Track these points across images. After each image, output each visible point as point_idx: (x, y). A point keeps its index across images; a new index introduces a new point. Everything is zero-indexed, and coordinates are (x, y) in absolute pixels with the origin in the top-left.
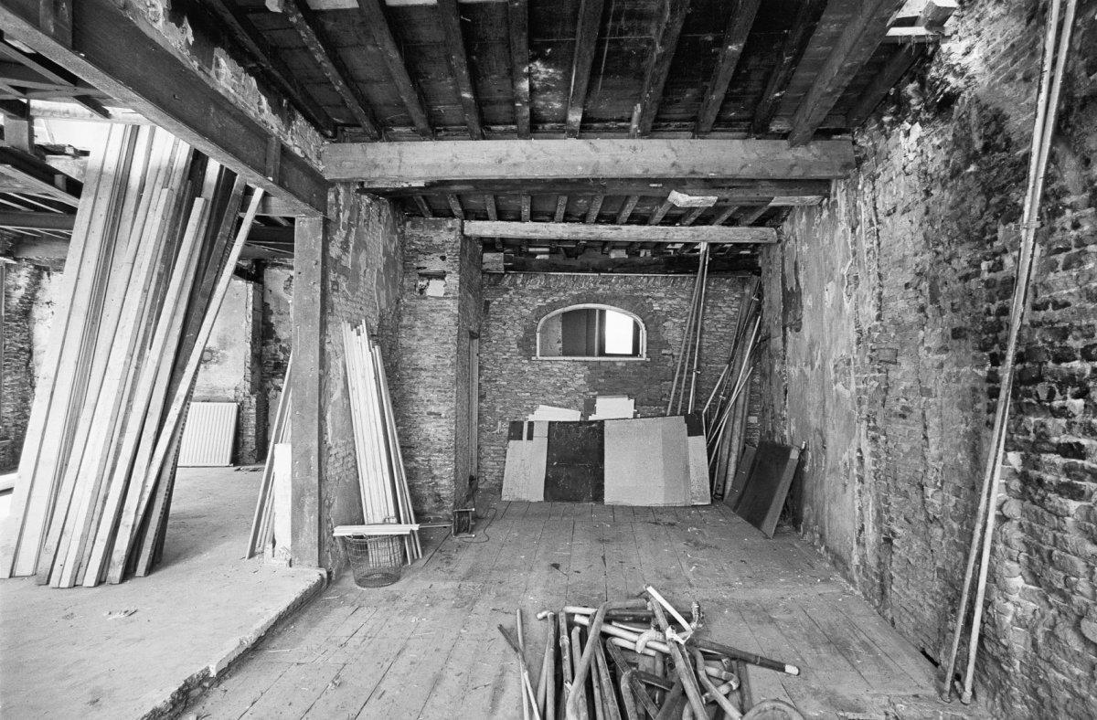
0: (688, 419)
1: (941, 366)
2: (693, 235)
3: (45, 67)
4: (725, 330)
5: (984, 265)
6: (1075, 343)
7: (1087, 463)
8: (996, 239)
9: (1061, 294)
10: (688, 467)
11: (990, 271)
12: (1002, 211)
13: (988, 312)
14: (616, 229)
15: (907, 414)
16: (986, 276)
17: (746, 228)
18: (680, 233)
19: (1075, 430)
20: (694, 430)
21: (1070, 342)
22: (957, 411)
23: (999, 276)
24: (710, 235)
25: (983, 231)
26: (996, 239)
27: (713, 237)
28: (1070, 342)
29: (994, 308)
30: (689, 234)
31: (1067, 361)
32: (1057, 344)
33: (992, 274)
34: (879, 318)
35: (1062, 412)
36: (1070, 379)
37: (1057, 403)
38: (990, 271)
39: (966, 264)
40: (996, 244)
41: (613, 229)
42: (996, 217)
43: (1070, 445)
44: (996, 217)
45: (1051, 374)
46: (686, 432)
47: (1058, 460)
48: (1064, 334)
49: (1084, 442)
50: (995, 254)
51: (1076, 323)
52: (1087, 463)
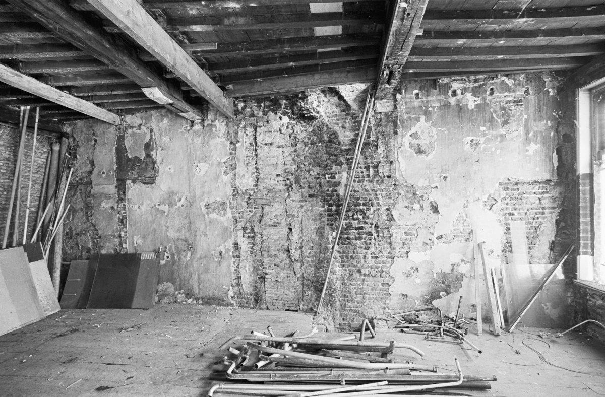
0: (27, 248)
1: (302, 206)
2: (77, 104)
3: (440, 39)
4: (36, 175)
5: (327, 176)
6: (361, 202)
7: (364, 231)
8: (332, 169)
9: (357, 189)
10: (34, 288)
11: (329, 178)
12: (336, 162)
13: (328, 190)
14: (17, 75)
15: (277, 225)
16: (328, 179)
17: (105, 111)
18: (69, 99)
19: (361, 223)
20: (34, 255)
21: (360, 201)
22: (311, 221)
23: (333, 180)
24: (87, 109)
25: (326, 166)
26: (332, 169)
27: (89, 111)
28: (360, 201)
29: (330, 190)
30: (75, 102)
31: (359, 206)
32: (355, 201)
33: (330, 179)
34: (256, 185)
35: (358, 219)
36: (361, 210)
37: (355, 217)
38: (329, 178)
39: (316, 174)
40: (331, 170)
41: (14, 73)
42: (333, 162)
43: (360, 227)
44: (333, 162)
45: (354, 209)
46: (27, 260)
47: (356, 232)
48: (358, 199)
49: (363, 226)
50: (332, 174)
51: (361, 196)
52: (364, 231)
